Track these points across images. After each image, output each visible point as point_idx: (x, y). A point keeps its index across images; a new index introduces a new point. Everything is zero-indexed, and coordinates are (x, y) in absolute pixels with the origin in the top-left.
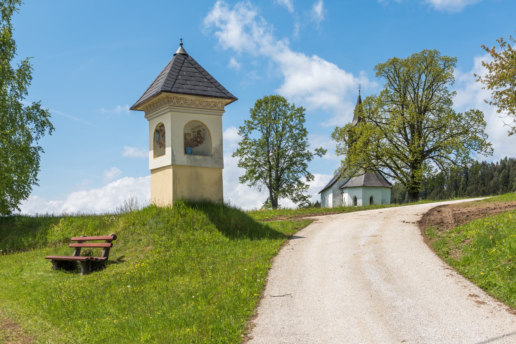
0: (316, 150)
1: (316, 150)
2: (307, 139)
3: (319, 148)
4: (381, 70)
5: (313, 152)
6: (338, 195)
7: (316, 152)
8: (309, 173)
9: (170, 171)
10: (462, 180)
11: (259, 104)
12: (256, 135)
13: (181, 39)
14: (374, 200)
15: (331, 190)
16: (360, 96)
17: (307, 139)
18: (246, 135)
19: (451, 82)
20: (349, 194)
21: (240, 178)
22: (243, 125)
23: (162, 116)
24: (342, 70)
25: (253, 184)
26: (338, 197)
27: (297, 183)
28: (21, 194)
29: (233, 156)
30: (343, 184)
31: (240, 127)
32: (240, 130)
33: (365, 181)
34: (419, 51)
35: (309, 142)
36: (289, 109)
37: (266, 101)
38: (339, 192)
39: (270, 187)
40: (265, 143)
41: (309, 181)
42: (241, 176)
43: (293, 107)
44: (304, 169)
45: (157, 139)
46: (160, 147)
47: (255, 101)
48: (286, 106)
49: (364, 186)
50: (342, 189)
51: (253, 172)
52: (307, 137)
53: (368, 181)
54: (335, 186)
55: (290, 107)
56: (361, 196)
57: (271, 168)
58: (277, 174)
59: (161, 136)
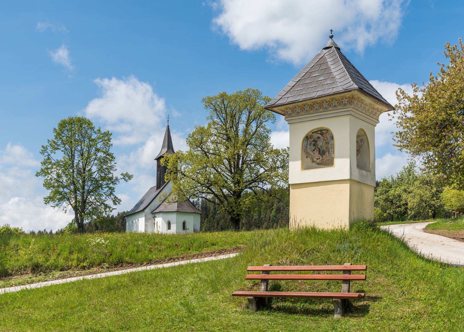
0: (122, 174)
1: (122, 174)
2: (115, 163)
3: (125, 173)
4: (209, 102)
5: (120, 177)
6: (150, 219)
7: (122, 177)
8: (115, 197)
9: (347, 187)
10: (212, 209)
11: (63, 125)
12: (59, 156)
13: (331, 31)
14: (186, 225)
15: (143, 214)
16: (168, 126)
17: (115, 163)
18: (49, 155)
19: (273, 121)
21: (45, 198)
22: (46, 144)
23: (321, 121)
25: (57, 205)
26: (150, 221)
27: (103, 206)
29: (37, 176)
30: (154, 209)
31: (43, 147)
32: (42, 149)
33: (178, 207)
34: (244, 89)
35: (117, 167)
36: (95, 132)
37: (71, 122)
38: (151, 216)
39: (75, 208)
40: (67, 166)
41: (116, 204)
42: (46, 197)
43: (99, 130)
44: (111, 193)
45: (305, 148)
46: (307, 157)
47: (59, 121)
48: (92, 128)
50: (154, 214)
51: (57, 192)
52: (115, 162)
53: (181, 207)
55: (95, 130)
58: (83, 197)
59: (309, 144)
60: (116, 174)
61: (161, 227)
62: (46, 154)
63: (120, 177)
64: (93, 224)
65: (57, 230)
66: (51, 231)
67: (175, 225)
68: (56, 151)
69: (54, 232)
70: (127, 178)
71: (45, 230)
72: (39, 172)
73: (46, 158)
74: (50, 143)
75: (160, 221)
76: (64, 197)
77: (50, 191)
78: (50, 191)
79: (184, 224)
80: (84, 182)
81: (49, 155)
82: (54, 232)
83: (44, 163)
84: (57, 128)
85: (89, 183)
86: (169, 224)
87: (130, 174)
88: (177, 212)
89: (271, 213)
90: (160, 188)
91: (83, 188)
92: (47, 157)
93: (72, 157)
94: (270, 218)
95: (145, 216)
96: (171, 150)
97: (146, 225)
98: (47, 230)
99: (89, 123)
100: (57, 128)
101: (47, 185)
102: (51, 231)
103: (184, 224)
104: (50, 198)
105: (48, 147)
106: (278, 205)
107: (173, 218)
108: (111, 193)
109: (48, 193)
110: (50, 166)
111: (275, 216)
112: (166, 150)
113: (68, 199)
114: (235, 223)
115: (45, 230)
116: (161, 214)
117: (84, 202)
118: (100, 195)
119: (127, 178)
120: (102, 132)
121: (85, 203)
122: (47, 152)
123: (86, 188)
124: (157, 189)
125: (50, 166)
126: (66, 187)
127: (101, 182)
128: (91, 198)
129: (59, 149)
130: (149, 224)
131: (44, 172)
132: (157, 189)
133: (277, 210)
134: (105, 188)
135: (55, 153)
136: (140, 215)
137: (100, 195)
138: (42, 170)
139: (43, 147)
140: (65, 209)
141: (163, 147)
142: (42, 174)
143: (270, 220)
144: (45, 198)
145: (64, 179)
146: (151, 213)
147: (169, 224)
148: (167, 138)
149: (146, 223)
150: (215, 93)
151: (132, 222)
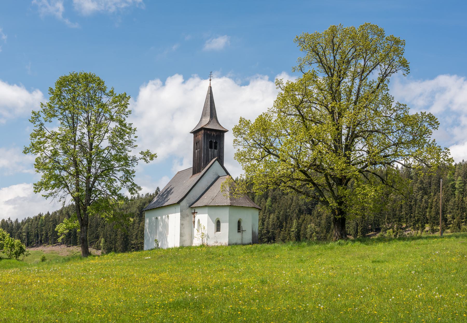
0: (142, 153)
2: (136, 137)
3: (145, 151)
4: (301, 41)
5: (138, 156)
6: (188, 216)
7: (142, 156)
11: (63, 83)
15: (178, 208)
16: (211, 87)
17: (136, 137)
20: (210, 216)
21: (35, 185)
22: (38, 108)
24: (16, 87)
26: (188, 218)
28: (72, 204)
30: (193, 201)
31: (33, 113)
32: (33, 115)
37: (75, 79)
38: (188, 211)
42: (36, 182)
43: (112, 92)
47: (57, 79)
48: (103, 90)
49: (231, 206)
50: (193, 208)
52: (135, 135)
54: (184, 203)
55: (107, 92)
56: (228, 219)
57: (78, 173)
58: (88, 182)
60: (132, 153)
61: (206, 228)
62: (38, 123)
63: (138, 156)
64: (64, 212)
65: (23, 219)
66: (17, 220)
67: (228, 224)
68: (53, 119)
69: (20, 221)
70: (148, 159)
71: (9, 219)
72: (29, 147)
73: (38, 128)
74: (44, 108)
75: (203, 219)
76: (60, 182)
77: (42, 174)
78: (42, 174)
79: (239, 223)
80: (90, 162)
81: (42, 124)
82: (20, 221)
83: (33, 136)
84: (54, 88)
85: (98, 165)
86: (218, 224)
87: (153, 153)
88: (231, 206)
89: (266, 202)
90: (199, 171)
91: (89, 171)
92: (39, 127)
93: (74, 129)
94: (266, 208)
95: (181, 211)
96: (214, 119)
97: (182, 225)
98: (11, 219)
99: (100, 83)
100: (54, 88)
101: (39, 165)
102: (17, 220)
103: (239, 223)
104: (41, 184)
105: (41, 113)
106: (274, 193)
107: (224, 215)
108: (127, 180)
109: (40, 176)
110: (42, 140)
111: (271, 206)
112: (208, 119)
113: (66, 186)
114: (340, 226)
115: (9, 219)
116: (206, 210)
117: (90, 190)
118: (111, 181)
119: (148, 159)
120: (117, 95)
121: (91, 192)
122: (39, 121)
123: (93, 170)
124: (194, 173)
125: (42, 140)
126: (64, 169)
127: (113, 163)
128: (100, 186)
129: (55, 116)
130: (186, 223)
131: (36, 147)
132: (194, 173)
133: (272, 199)
134: (119, 171)
135: (50, 122)
136: (172, 209)
137: (111, 181)
138: (33, 145)
139: (33, 113)
140: (63, 200)
141: (204, 115)
142: (33, 150)
143: (265, 210)
144: (35, 185)
145: (62, 158)
146: (190, 206)
147: (218, 224)
148: (209, 103)
149: (182, 222)
150: (320, 27)
151: (157, 218)
